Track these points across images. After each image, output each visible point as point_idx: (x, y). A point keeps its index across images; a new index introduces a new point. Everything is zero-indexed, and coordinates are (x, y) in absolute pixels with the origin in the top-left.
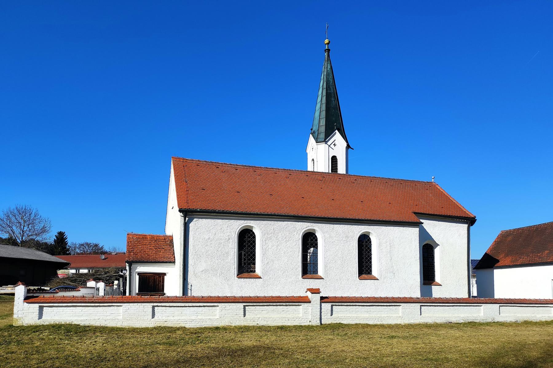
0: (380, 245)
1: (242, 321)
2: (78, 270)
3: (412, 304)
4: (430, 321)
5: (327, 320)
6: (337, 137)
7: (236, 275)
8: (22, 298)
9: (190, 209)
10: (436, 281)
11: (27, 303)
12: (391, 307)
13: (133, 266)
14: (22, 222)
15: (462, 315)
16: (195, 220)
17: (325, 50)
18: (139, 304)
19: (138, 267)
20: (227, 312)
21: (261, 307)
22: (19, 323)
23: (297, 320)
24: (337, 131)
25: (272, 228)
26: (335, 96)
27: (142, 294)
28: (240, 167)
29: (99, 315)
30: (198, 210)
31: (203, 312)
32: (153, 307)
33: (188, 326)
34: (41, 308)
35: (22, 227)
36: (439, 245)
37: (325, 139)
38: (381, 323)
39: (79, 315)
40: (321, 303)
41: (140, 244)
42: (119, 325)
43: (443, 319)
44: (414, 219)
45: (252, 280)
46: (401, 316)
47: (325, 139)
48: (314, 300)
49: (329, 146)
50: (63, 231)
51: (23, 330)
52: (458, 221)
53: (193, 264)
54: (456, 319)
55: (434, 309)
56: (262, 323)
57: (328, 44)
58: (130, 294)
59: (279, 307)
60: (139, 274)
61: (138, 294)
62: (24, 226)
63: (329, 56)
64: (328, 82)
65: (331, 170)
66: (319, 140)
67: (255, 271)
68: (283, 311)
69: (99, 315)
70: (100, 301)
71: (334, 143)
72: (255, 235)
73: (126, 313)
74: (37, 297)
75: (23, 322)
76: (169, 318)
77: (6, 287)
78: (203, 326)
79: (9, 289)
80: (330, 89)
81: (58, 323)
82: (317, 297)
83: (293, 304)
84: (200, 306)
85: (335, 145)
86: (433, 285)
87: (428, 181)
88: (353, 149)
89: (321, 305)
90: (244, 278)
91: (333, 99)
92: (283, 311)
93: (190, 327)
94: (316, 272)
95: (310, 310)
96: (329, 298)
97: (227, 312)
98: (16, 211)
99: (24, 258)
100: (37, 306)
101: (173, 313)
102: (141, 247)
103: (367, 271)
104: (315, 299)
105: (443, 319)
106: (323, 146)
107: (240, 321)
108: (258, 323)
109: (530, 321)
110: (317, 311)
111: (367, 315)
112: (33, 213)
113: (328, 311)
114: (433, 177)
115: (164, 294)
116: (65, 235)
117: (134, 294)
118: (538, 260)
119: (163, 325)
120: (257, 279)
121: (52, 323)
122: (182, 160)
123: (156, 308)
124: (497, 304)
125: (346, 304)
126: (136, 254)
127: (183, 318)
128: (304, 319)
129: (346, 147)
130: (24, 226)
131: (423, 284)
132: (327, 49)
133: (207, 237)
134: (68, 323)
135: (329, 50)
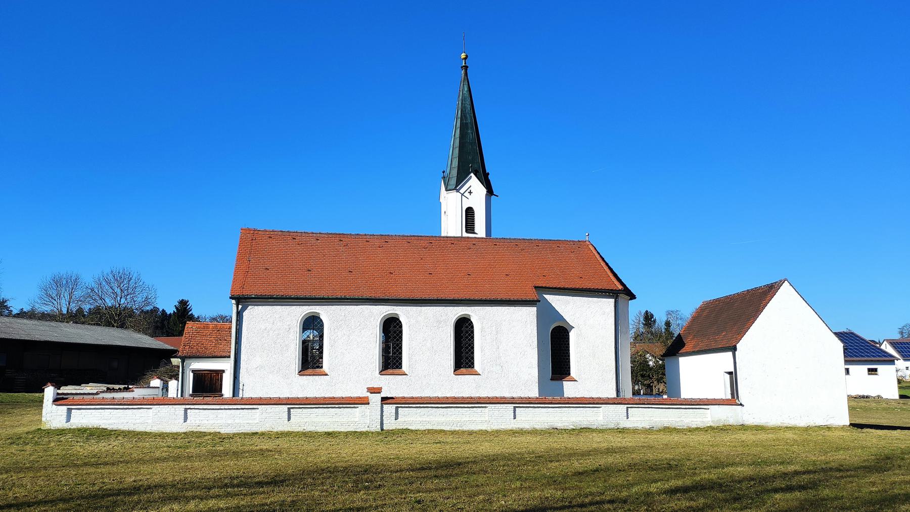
0: (482, 330)
1: (286, 426)
3: (502, 405)
4: (527, 426)
6: (474, 182)
7: (297, 372)
8: (51, 400)
9: (243, 295)
10: (571, 375)
11: (56, 405)
12: (475, 409)
13: (187, 362)
14: (118, 291)
15: (574, 419)
16: (250, 307)
17: (462, 67)
18: (171, 406)
19: (192, 363)
20: (269, 415)
21: (309, 410)
22: (47, 427)
23: (353, 424)
24: (472, 174)
25: (343, 314)
26: (473, 127)
27: (196, 395)
28: (324, 235)
29: (127, 418)
30: (253, 296)
31: (240, 416)
32: (186, 410)
33: (222, 431)
34: (69, 411)
35: (119, 298)
36: (574, 328)
37: (456, 186)
38: (461, 429)
39: (107, 418)
40: (382, 404)
41: (198, 335)
42: (148, 430)
43: (545, 424)
44: (533, 295)
45: (317, 377)
46: (487, 419)
48: (373, 401)
49: (462, 195)
50: (186, 299)
51: (48, 433)
52: (600, 295)
53: (246, 360)
54: (564, 424)
55: (533, 411)
57: (465, 59)
58: (182, 396)
59: (330, 409)
60: (193, 371)
61: (191, 395)
62: (121, 298)
63: (466, 74)
64: (464, 110)
65: (99, 329)
66: (449, 188)
67: (322, 366)
68: (336, 414)
69: (127, 418)
70: (129, 403)
71: (469, 191)
72: (323, 323)
73: (156, 416)
74: (67, 398)
75: (51, 425)
76: (203, 422)
77: (85, 386)
78: (241, 432)
79: (88, 388)
81: (85, 427)
83: (458, 405)
84: (237, 409)
85: (470, 193)
86: (564, 381)
87: (580, 240)
88: (497, 196)
90: (307, 375)
92: (336, 414)
93: (225, 432)
95: (368, 414)
96: (394, 399)
97: (269, 415)
98: (111, 277)
99: (114, 344)
100: (65, 408)
101: (207, 416)
102: (199, 338)
103: (467, 363)
104: (375, 399)
105: (545, 424)
106: (454, 196)
107: (284, 426)
108: (305, 428)
109: (673, 427)
110: (378, 414)
111: (442, 419)
112: (134, 278)
113: (391, 414)
114: (587, 234)
115: (222, 395)
116: (188, 305)
117: (187, 396)
118: (714, 346)
119: (195, 430)
120: (322, 376)
121: (80, 426)
122: (252, 232)
123: (189, 411)
124: (623, 406)
125: (414, 406)
126: (192, 348)
127: (219, 422)
128: (361, 424)
129: (486, 194)
130: (121, 298)
131: (551, 380)
132: (464, 66)
133: (263, 328)
134: (95, 426)
135: (466, 67)
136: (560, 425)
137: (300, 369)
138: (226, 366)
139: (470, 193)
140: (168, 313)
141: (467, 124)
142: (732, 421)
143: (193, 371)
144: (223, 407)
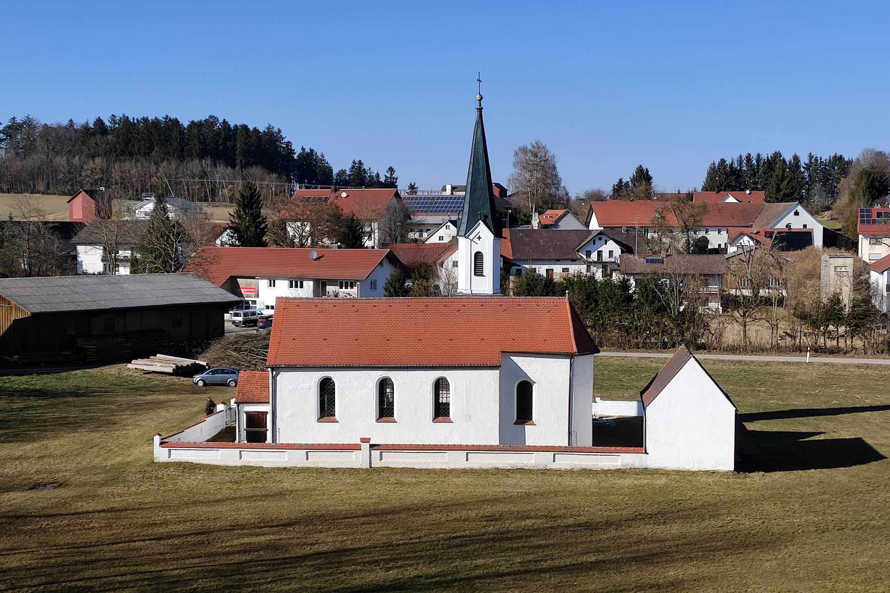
2: (294, 282)
5: (376, 463)
15: (511, 462)
16: (281, 373)
24: (480, 221)
30: (283, 366)
32: (240, 451)
33: (264, 466)
37: (465, 234)
42: (218, 464)
47: (465, 234)
49: (472, 240)
56: (321, 465)
60: (246, 413)
80: (478, 164)
82: (367, 445)
85: (479, 238)
89: (370, 452)
91: (481, 177)
94: (392, 415)
104: (365, 447)
121: (176, 461)
136: (501, 466)
137: (319, 417)
138: (267, 408)
139: (479, 238)
140: (232, 126)
141: (478, 169)
142: (637, 465)
143: (246, 413)
144: (263, 450)
